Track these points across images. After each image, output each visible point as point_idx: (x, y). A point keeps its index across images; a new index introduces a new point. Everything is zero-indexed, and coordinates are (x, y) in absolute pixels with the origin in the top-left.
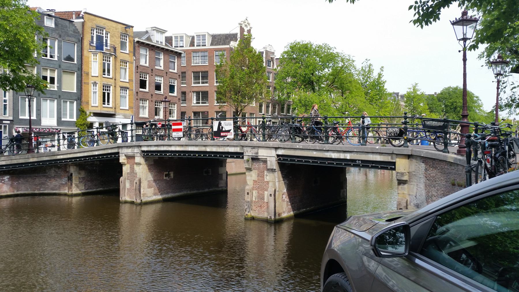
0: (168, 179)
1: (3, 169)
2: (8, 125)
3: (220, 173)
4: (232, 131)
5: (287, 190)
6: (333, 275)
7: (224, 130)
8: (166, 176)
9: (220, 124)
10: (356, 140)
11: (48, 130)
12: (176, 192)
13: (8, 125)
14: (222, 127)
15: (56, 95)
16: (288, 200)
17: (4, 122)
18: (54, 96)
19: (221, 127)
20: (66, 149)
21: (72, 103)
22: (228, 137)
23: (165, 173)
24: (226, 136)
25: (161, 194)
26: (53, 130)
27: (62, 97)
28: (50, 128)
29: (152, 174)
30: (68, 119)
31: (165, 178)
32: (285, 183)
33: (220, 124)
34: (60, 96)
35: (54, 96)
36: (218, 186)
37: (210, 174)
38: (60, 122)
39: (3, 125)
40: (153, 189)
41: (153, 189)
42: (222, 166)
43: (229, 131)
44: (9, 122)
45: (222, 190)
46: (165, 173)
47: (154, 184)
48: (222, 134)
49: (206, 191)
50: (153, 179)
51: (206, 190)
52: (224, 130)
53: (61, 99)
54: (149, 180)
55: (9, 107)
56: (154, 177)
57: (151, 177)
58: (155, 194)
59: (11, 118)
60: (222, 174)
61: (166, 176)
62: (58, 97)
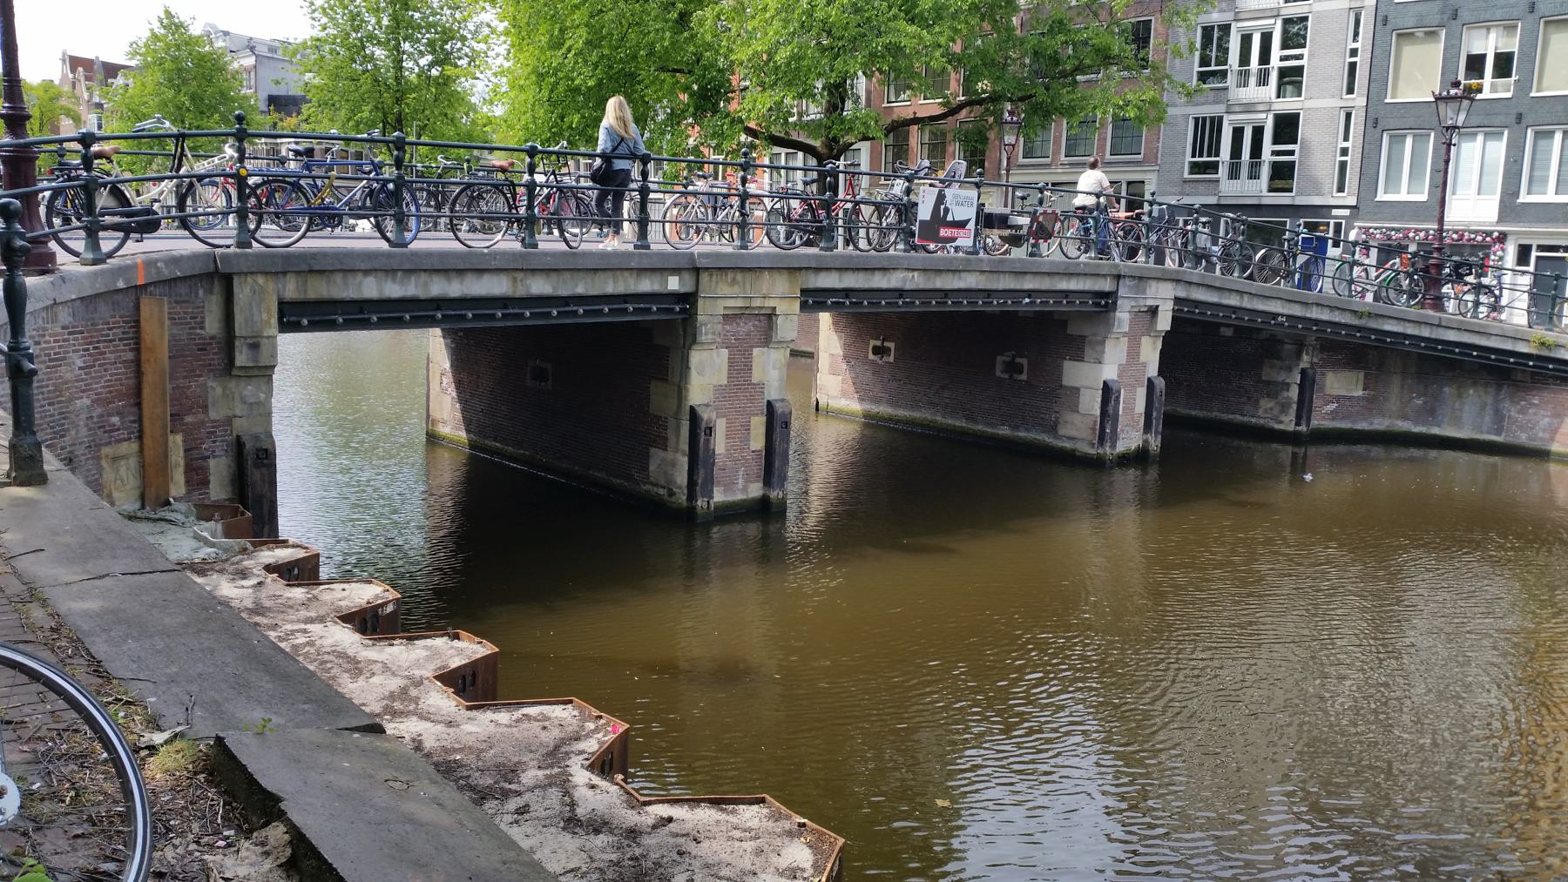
0: (880, 362)
1: (1490, 359)
2: (1344, 222)
3: (1066, 381)
4: (971, 226)
5: (451, 366)
6: (533, 711)
7: (949, 218)
8: (876, 351)
9: (941, 198)
10: (901, 246)
11: (1455, 236)
12: (900, 407)
13: (1344, 222)
14: (947, 210)
15: (1507, 114)
16: (454, 394)
17: (1335, 212)
18: (1497, 120)
19: (942, 207)
20: (384, 245)
21: (1420, 139)
22: (957, 243)
23: (873, 343)
24: (954, 239)
25: (861, 400)
26: (1473, 236)
27: (1527, 120)
28: (1464, 231)
29: (840, 338)
30: (1403, 196)
31: (871, 356)
32: (446, 345)
33: (941, 198)
34: (1519, 118)
35: (1497, 120)
36: (1056, 432)
37: (1024, 377)
38: (1510, 208)
39: (1332, 222)
40: (840, 378)
41: (840, 378)
42: (1079, 357)
43: (962, 225)
44: (1347, 212)
45: (1074, 451)
46: (873, 343)
47: (844, 366)
48: (943, 232)
49: (1000, 432)
50: (842, 354)
51: (1004, 431)
52: (949, 218)
53: (1524, 124)
54: (833, 352)
55: (1352, 169)
56: (846, 346)
57: (838, 345)
58: (844, 394)
59: (1352, 201)
60: (1077, 390)
61: (874, 353)
62: (1512, 119)
